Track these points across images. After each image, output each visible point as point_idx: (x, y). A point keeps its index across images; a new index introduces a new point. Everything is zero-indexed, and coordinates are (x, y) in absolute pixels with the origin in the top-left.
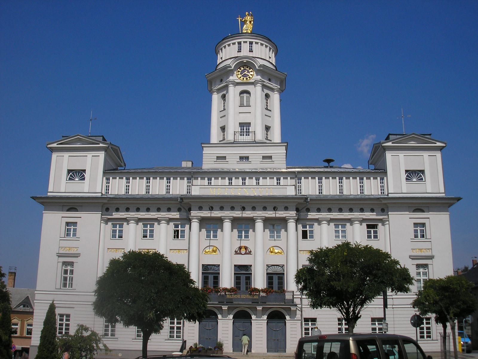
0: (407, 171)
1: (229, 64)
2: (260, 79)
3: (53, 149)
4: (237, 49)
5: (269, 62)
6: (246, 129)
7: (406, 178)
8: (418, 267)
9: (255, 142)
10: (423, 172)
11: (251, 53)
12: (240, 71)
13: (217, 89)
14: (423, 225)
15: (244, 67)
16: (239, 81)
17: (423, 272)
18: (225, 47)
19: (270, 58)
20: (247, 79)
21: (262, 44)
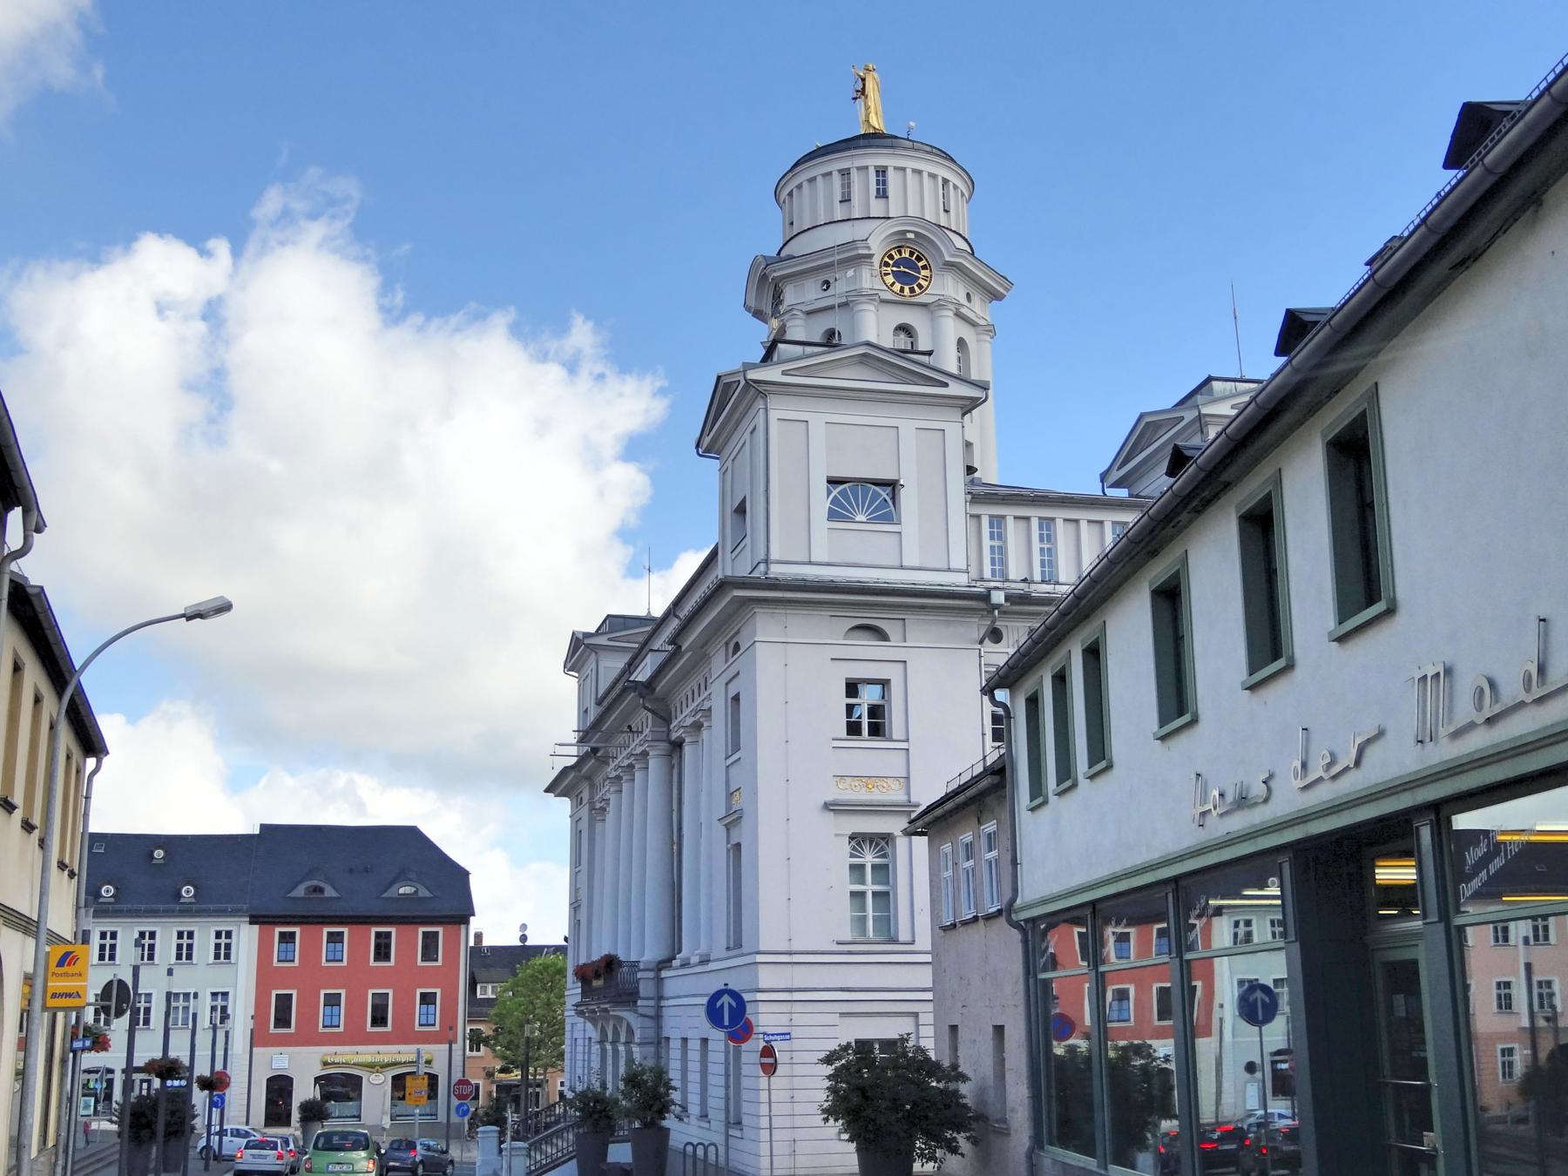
8: (859, 844)
10: (892, 485)
16: (888, 296)
17: (874, 867)
18: (790, 194)
20: (912, 290)
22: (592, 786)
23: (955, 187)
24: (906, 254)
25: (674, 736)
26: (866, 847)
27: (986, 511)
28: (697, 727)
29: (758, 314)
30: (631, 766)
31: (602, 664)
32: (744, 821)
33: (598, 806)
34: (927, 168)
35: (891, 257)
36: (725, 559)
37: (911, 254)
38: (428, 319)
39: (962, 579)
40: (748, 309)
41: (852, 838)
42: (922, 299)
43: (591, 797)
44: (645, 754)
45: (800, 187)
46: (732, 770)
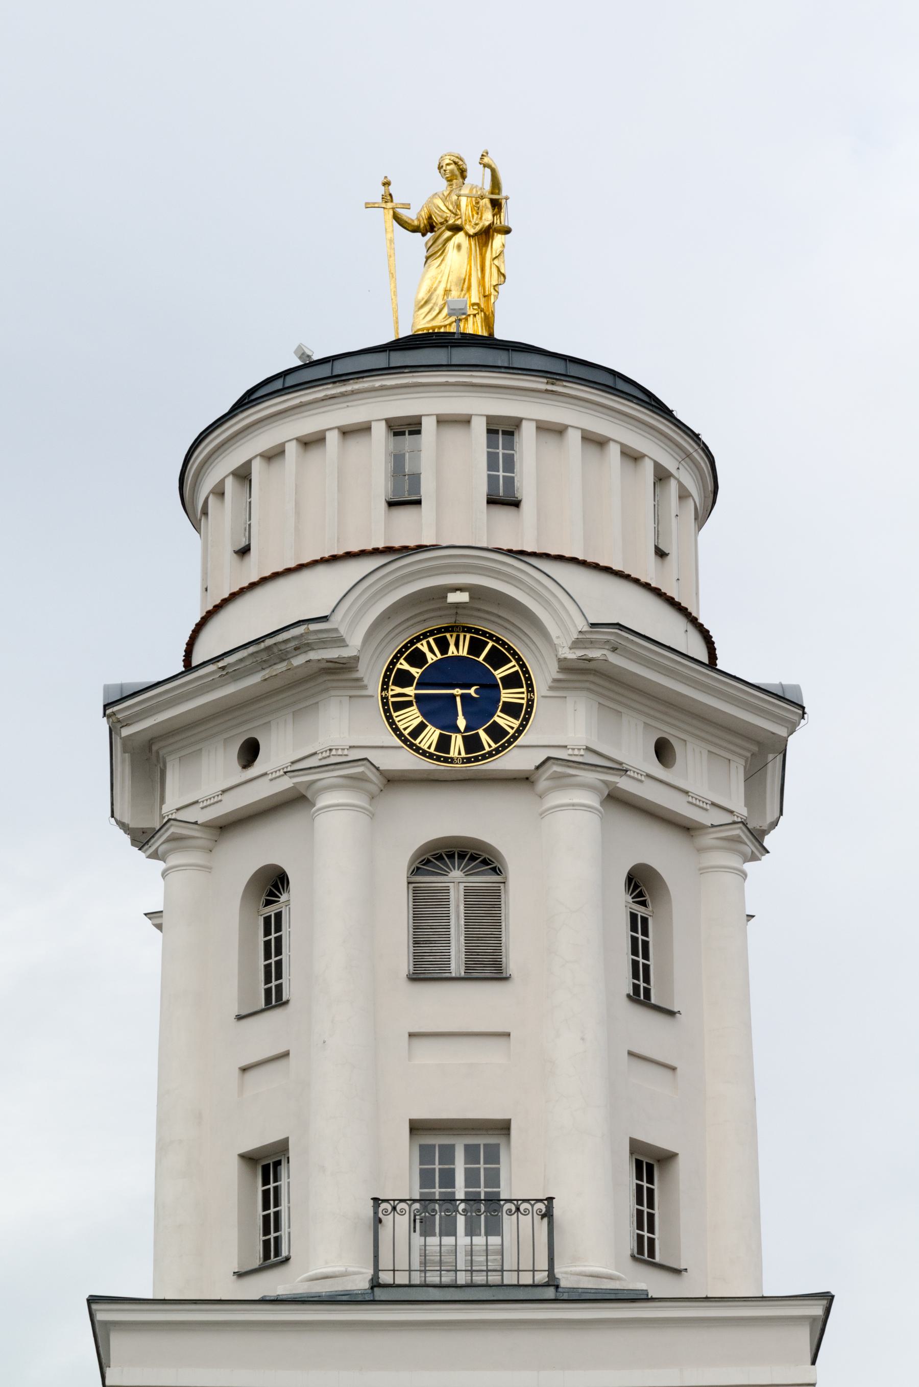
1: (324, 619)
2: (588, 749)
4: (380, 486)
5: (657, 592)
6: (448, 1178)
9: (550, 1293)
11: (503, 514)
12: (416, 672)
13: (207, 825)
15: (452, 642)
16: (405, 760)
18: (243, 475)
19: (661, 554)
21: (632, 457)
24: (459, 649)
35: (417, 659)
37: (476, 647)
42: (513, 760)
45: (274, 455)
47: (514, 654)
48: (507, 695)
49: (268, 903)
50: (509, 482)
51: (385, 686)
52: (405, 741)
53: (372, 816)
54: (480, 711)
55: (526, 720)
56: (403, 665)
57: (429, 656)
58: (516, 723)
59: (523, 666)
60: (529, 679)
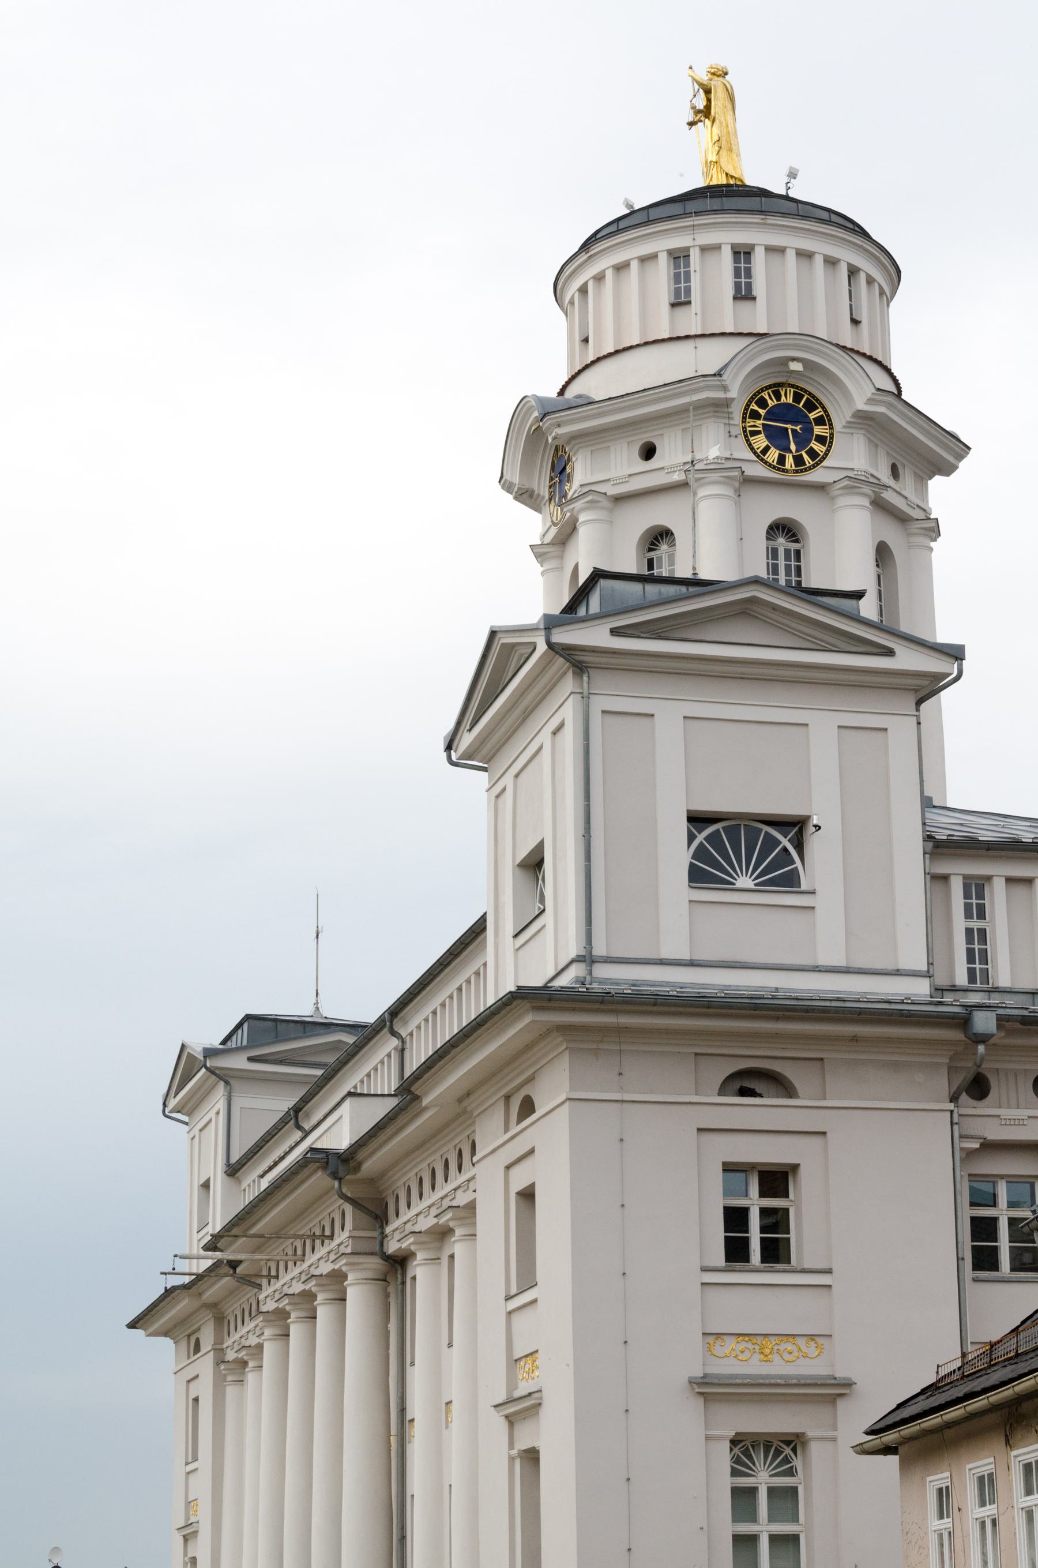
0: (697, 820)
3: (588, 658)
7: (691, 864)
8: (747, 1453)
10: (796, 827)
12: (762, 412)
14: (776, 1180)
15: (783, 393)
16: (759, 471)
17: (772, 1491)
18: (583, 290)
19: (855, 322)
21: (831, 262)
22: (220, 1320)
23: (870, 281)
25: (392, 1247)
26: (759, 1458)
27: (958, 869)
28: (442, 1234)
29: (526, 496)
30: (308, 1297)
31: (238, 1102)
32: (545, 1412)
33: (231, 1355)
34: (821, 247)
35: (762, 403)
36: (499, 943)
37: (797, 398)
38: (545, 987)
39: (921, 989)
40: (507, 487)
41: (734, 1442)
43: (219, 1340)
44: (338, 1277)
45: (600, 278)
46: (515, 1317)
47: (821, 404)
48: (818, 430)
49: (650, 550)
50: (749, 286)
51: (744, 420)
52: (758, 456)
53: (738, 505)
54: (802, 441)
55: (830, 447)
56: (754, 407)
57: (769, 401)
58: (824, 449)
59: (826, 411)
60: (830, 420)
